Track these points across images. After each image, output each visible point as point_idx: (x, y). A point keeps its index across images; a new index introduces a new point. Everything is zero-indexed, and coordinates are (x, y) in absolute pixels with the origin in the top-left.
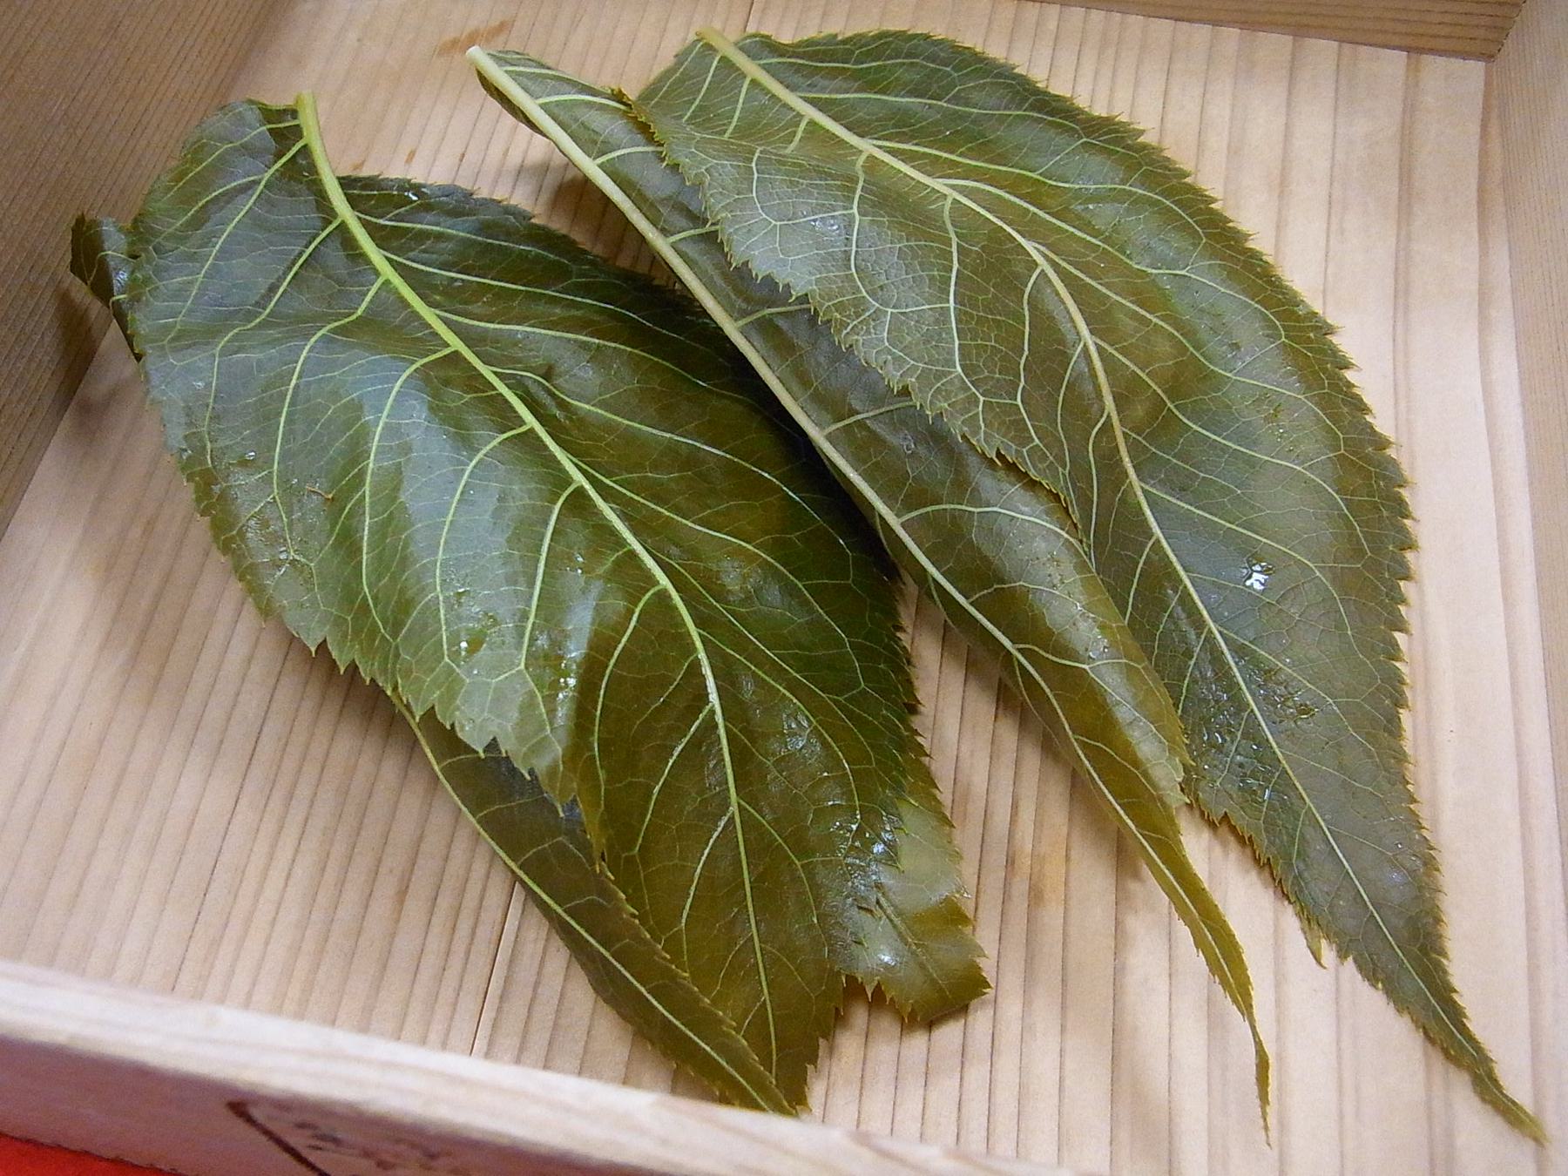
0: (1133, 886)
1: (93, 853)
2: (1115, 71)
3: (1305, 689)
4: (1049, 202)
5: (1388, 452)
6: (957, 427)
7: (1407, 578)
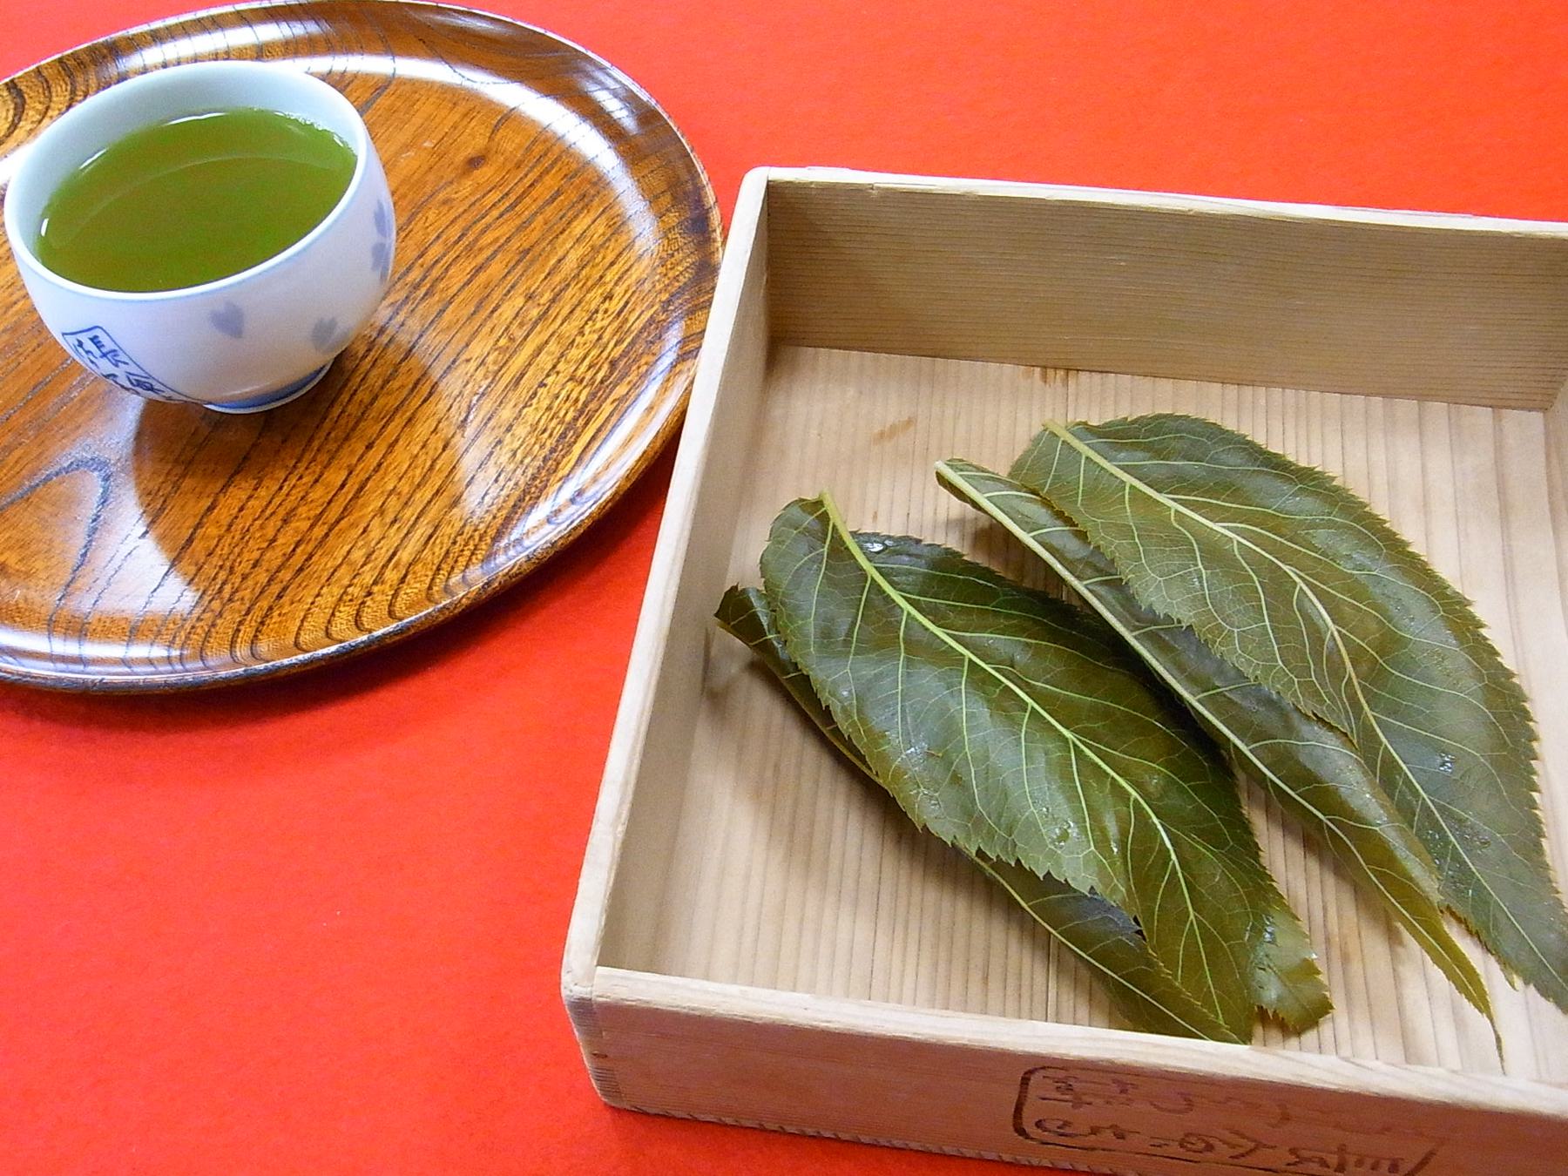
0: (1400, 950)
1: (797, 967)
2: (1308, 431)
3: (1486, 830)
4: (1284, 531)
5: (1515, 680)
6: (1288, 700)
7: (1535, 758)
